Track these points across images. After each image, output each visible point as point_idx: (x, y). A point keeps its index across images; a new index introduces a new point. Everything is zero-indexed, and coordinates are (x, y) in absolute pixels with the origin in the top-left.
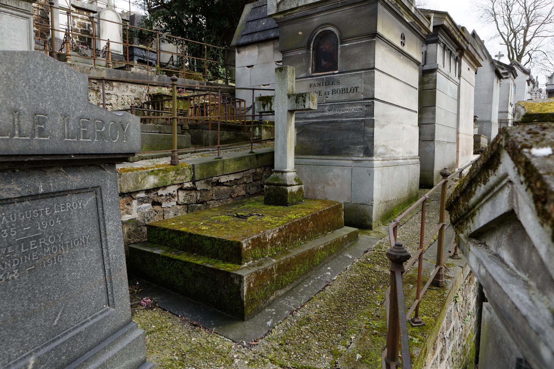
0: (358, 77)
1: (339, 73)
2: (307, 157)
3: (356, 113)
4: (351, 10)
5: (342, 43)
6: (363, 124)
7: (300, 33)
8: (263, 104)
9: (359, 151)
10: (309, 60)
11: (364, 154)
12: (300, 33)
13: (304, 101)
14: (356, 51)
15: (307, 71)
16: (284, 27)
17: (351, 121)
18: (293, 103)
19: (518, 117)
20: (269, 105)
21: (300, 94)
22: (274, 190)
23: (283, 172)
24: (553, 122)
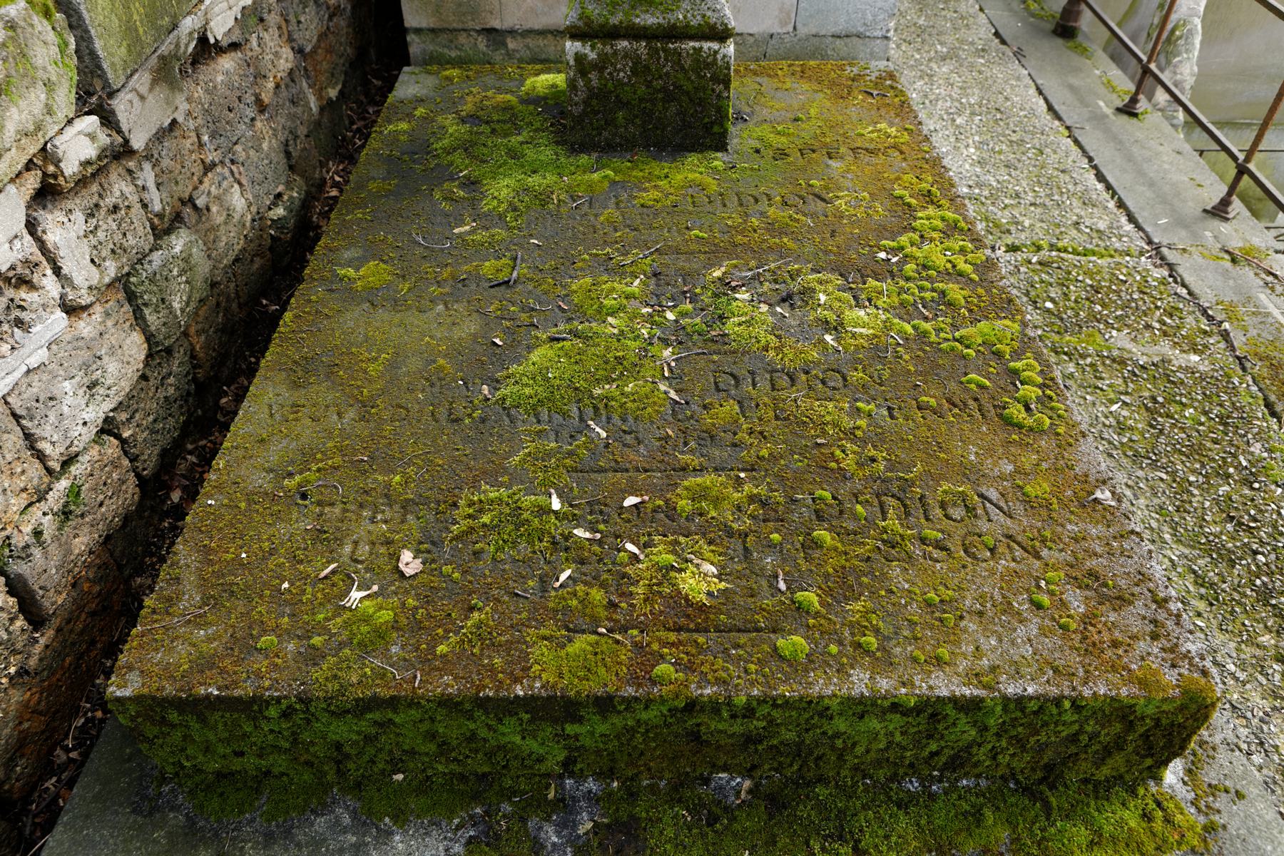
22: (639, 69)
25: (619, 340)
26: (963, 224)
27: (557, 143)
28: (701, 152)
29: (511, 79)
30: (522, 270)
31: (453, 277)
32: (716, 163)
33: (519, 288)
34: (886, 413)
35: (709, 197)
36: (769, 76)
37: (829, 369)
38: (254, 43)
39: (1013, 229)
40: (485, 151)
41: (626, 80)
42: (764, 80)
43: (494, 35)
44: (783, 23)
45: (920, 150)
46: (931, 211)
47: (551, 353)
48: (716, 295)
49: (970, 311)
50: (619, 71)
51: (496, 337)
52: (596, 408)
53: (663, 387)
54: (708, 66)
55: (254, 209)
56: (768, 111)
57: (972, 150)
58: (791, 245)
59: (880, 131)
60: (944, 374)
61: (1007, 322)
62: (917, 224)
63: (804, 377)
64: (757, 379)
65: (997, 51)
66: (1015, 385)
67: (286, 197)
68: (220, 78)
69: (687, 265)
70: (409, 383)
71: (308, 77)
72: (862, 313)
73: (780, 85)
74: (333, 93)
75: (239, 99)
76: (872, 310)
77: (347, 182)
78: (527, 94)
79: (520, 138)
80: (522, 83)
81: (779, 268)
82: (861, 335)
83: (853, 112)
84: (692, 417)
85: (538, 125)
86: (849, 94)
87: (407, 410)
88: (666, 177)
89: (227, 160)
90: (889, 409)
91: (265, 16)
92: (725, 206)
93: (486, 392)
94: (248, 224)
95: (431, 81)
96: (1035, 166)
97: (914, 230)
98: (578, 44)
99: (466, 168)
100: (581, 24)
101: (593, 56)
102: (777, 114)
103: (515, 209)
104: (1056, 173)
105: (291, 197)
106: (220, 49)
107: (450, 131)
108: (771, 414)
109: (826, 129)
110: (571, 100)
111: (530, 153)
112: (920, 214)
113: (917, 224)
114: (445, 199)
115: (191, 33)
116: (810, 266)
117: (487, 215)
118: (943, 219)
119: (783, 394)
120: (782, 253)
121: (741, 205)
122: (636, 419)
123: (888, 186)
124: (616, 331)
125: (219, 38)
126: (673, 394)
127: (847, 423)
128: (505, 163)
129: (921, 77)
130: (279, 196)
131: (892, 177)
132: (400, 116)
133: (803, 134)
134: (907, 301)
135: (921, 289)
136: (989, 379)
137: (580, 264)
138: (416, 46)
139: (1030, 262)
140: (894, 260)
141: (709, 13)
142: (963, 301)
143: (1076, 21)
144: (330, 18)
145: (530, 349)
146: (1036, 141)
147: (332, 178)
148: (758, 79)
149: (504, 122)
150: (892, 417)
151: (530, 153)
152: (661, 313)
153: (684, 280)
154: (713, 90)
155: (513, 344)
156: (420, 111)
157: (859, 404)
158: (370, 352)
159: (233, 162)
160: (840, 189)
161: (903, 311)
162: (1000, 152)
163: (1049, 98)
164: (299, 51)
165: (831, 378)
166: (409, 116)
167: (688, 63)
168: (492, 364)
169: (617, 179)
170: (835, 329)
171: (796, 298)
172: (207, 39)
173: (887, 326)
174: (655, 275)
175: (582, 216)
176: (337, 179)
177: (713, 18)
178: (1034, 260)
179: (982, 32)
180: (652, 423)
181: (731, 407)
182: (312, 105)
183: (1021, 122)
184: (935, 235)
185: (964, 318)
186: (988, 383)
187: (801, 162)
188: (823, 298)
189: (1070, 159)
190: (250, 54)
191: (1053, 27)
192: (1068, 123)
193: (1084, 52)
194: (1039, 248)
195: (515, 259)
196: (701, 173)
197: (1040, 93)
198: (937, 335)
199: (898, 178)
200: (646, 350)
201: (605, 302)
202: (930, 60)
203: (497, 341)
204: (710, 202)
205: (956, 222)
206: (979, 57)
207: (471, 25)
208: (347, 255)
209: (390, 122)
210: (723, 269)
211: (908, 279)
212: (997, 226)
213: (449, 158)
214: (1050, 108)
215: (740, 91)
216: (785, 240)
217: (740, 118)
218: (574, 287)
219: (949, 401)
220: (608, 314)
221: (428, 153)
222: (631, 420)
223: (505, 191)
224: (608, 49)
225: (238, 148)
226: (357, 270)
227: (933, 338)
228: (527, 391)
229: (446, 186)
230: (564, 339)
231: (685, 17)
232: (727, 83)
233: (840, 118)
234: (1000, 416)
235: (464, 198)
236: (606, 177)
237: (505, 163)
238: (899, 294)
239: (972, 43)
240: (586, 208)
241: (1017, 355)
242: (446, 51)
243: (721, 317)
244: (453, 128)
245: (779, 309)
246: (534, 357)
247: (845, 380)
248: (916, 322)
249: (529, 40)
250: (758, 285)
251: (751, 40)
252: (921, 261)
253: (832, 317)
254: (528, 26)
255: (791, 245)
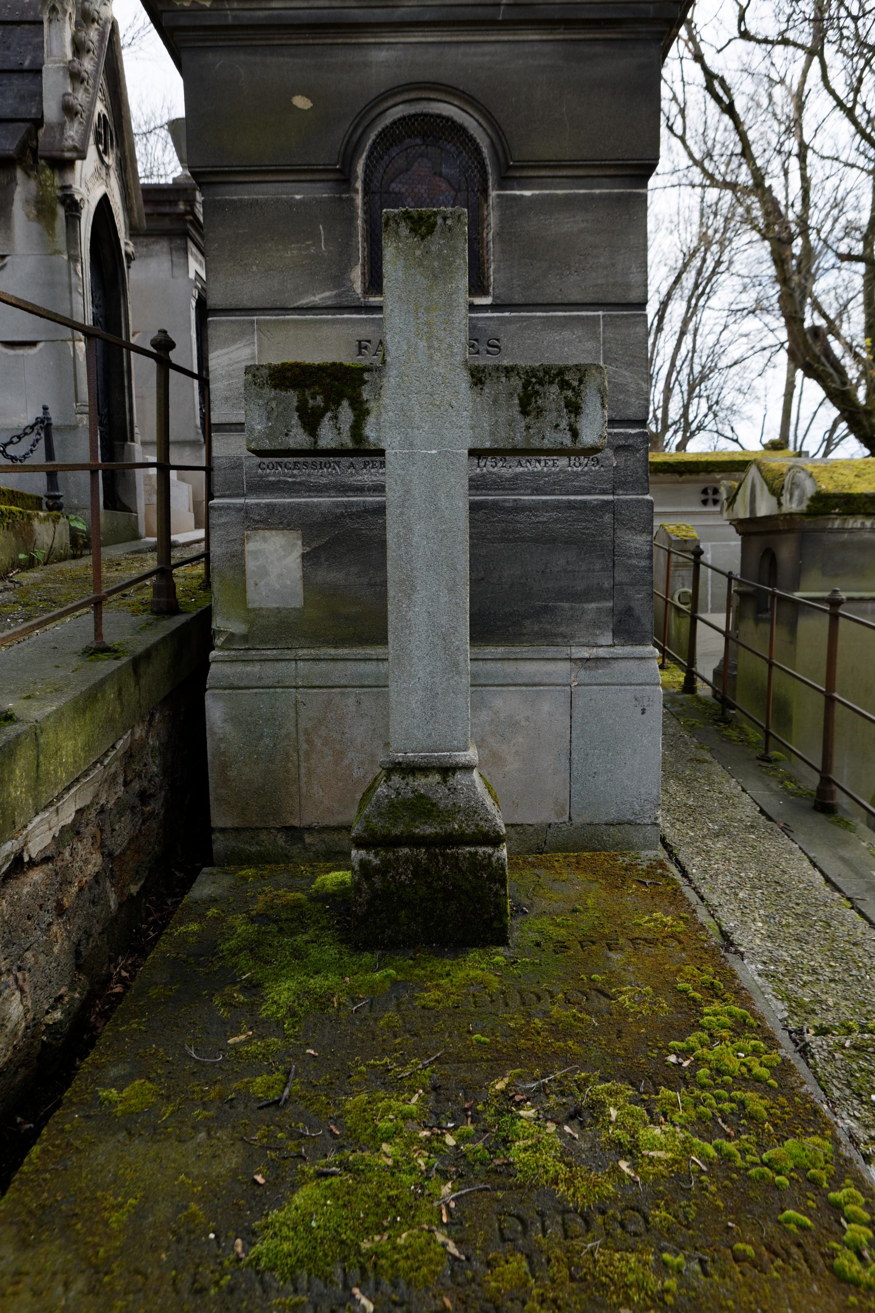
0: (579, 332)
1: (493, 307)
2: (360, 652)
3: (577, 475)
4: (547, 48)
5: (504, 182)
6: (608, 518)
7: (301, 102)
8: (302, 409)
9: (596, 624)
10: (350, 235)
11: (615, 634)
12: (301, 102)
13: (575, 408)
14: (569, 224)
15: (339, 279)
16: (210, 57)
17: (557, 506)
18: (503, 415)
19: (800, 502)
20: (346, 414)
21: (547, 370)
22: (420, 871)
23: (447, 770)
24: (868, 515)
25: (393, 1174)
26: (752, 1021)
27: (342, 941)
28: (483, 947)
29: (303, 877)
30: (295, 1086)
31: (221, 1096)
32: (498, 958)
33: (290, 1108)
34: (697, 1268)
35: (491, 996)
36: (547, 868)
37: (627, 1208)
38: (67, 853)
39: (817, 1008)
40: (270, 951)
41: (407, 882)
42: (542, 872)
43: (294, 833)
44: (559, 814)
45: (698, 940)
46: (717, 1006)
47: (317, 1193)
48: (499, 1113)
49: (775, 1125)
50: (401, 874)
51: (258, 1173)
52: (363, 1269)
53: (440, 1238)
54: (484, 867)
55: (30, 1016)
56: (549, 903)
57: (760, 924)
58: (576, 1048)
59: (656, 920)
60: (758, 1211)
61: (817, 1139)
62: (705, 1020)
63: (599, 1219)
64: (548, 1223)
65: (765, 827)
66: (841, 1224)
67: (66, 999)
68: (26, 890)
69: (469, 1076)
70: (153, 1238)
71: (113, 877)
72: (657, 1131)
73: (557, 876)
74: (134, 889)
75: (41, 907)
76: (668, 1128)
77: (133, 977)
78: (317, 891)
79: (306, 937)
80: (313, 880)
81: (566, 1077)
82: (659, 1160)
83: (628, 901)
84: (473, 1279)
85: (324, 923)
86: (623, 882)
87: (146, 1277)
88: (448, 975)
89: (15, 968)
90: (702, 1262)
91: (82, 830)
92: (507, 1005)
93: (239, 1249)
94: (20, 1033)
95: (226, 881)
96: (825, 939)
97: (702, 1028)
98: (363, 852)
99: (250, 970)
100: (365, 835)
101: (376, 861)
102: (556, 905)
103: (294, 1015)
104: (848, 946)
105: (72, 999)
106: (33, 864)
107: (239, 931)
108: (565, 1272)
109: (604, 920)
110: (356, 901)
111: (314, 952)
112: (706, 1010)
113: (705, 1020)
114: (224, 1005)
115: (8, 856)
116: (597, 1073)
117: (264, 1022)
118: (730, 1015)
119: (577, 1243)
120: (567, 1059)
121: (524, 1004)
122: (409, 1284)
123: (670, 979)
124: (390, 1162)
125: (33, 856)
126: (452, 1248)
127: (654, 1284)
128: (289, 964)
129: (698, 854)
130: (61, 997)
131: (673, 968)
132: (192, 917)
133: (582, 926)
134: (706, 1115)
135: (719, 1099)
136: (810, 1217)
137: (356, 1078)
138: (219, 844)
139: (843, 1047)
140: (686, 1064)
141: (482, 823)
142: (765, 1114)
143: (832, 799)
144: (144, 823)
145: (294, 1187)
146: (821, 913)
147: (119, 972)
148: (536, 871)
149: (291, 920)
150: (706, 1273)
151: (314, 952)
152: (440, 1138)
153: (465, 1094)
154: (490, 889)
155: (274, 1183)
156: (212, 912)
157: (666, 1256)
158: (116, 1196)
159: (20, 969)
160: (622, 983)
161: (702, 1128)
162: (788, 925)
163: (824, 870)
164: (109, 856)
165: (625, 1219)
166: (201, 917)
167: (465, 866)
168: (251, 1209)
169: (399, 978)
170: (630, 1153)
171: (585, 1114)
172: (22, 858)
173: (687, 1149)
174: (435, 1088)
175: (361, 1021)
176: (124, 974)
177: (485, 826)
178: (847, 1044)
179: (747, 811)
180: (428, 1289)
181: (518, 1265)
182: (112, 903)
183: (802, 894)
184: (725, 1033)
185: (770, 1135)
186: (809, 1222)
187: (582, 955)
188: (613, 1113)
189: (859, 931)
190: (60, 864)
191: (812, 804)
192: (849, 894)
193: (847, 826)
194: (850, 1031)
195: (287, 1073)
196: (483, 970)
197: (815, 865)
198: (743, 1158)
199: (680, 970)
200: (423, 1187)
201: (380, 1125)
202: (704, 837)
203: (260, 1179)
204: (492, 1001)
205: (744, 1018)
206: (750, 833)
207: (272, 824)
208: (114, 1072)
209: (181, 924)
210: (506, 1080)
211: (703, 1087)
212: (801, 1005)
213: (234, 960)
214: (828, 880)
215: (517, 884)
216: (570, 1043)
217: (519, 910)
218: (348, 1107)
219: (769, 1248)
220: (382, 1140)
221: (214, 955)
222: (402, 1284)
223: (286, 994)
224: (390, 855)
225: (29, 954)
226: (120, 1091)
227: (739, 1162)
228: (286, 1246)
229: (227, 990)
230: (333, 1174)
231: (460, 827)
232: (503, 882)
233: (617, 908)
234: (831, 1268)
235: (243, 1003)
236: (388, 976)
237: (289, 964)
238: (695, 1106)
239: (741, 820)
240: (366, 1012)
241: (836, 1183)
242: (247, 847)
243: (505, 1141)
244: (242, 927)
245: (567, 1129)
246: (298, 1199)
247: (647, 1221)
248: (718, 1141)
249: (325, 835)
250: (544, 1099)
251: (532, 829)
252: (713, 1064)
253: (625, 1138)
254: (325, 822)
255: (576, 1048)
